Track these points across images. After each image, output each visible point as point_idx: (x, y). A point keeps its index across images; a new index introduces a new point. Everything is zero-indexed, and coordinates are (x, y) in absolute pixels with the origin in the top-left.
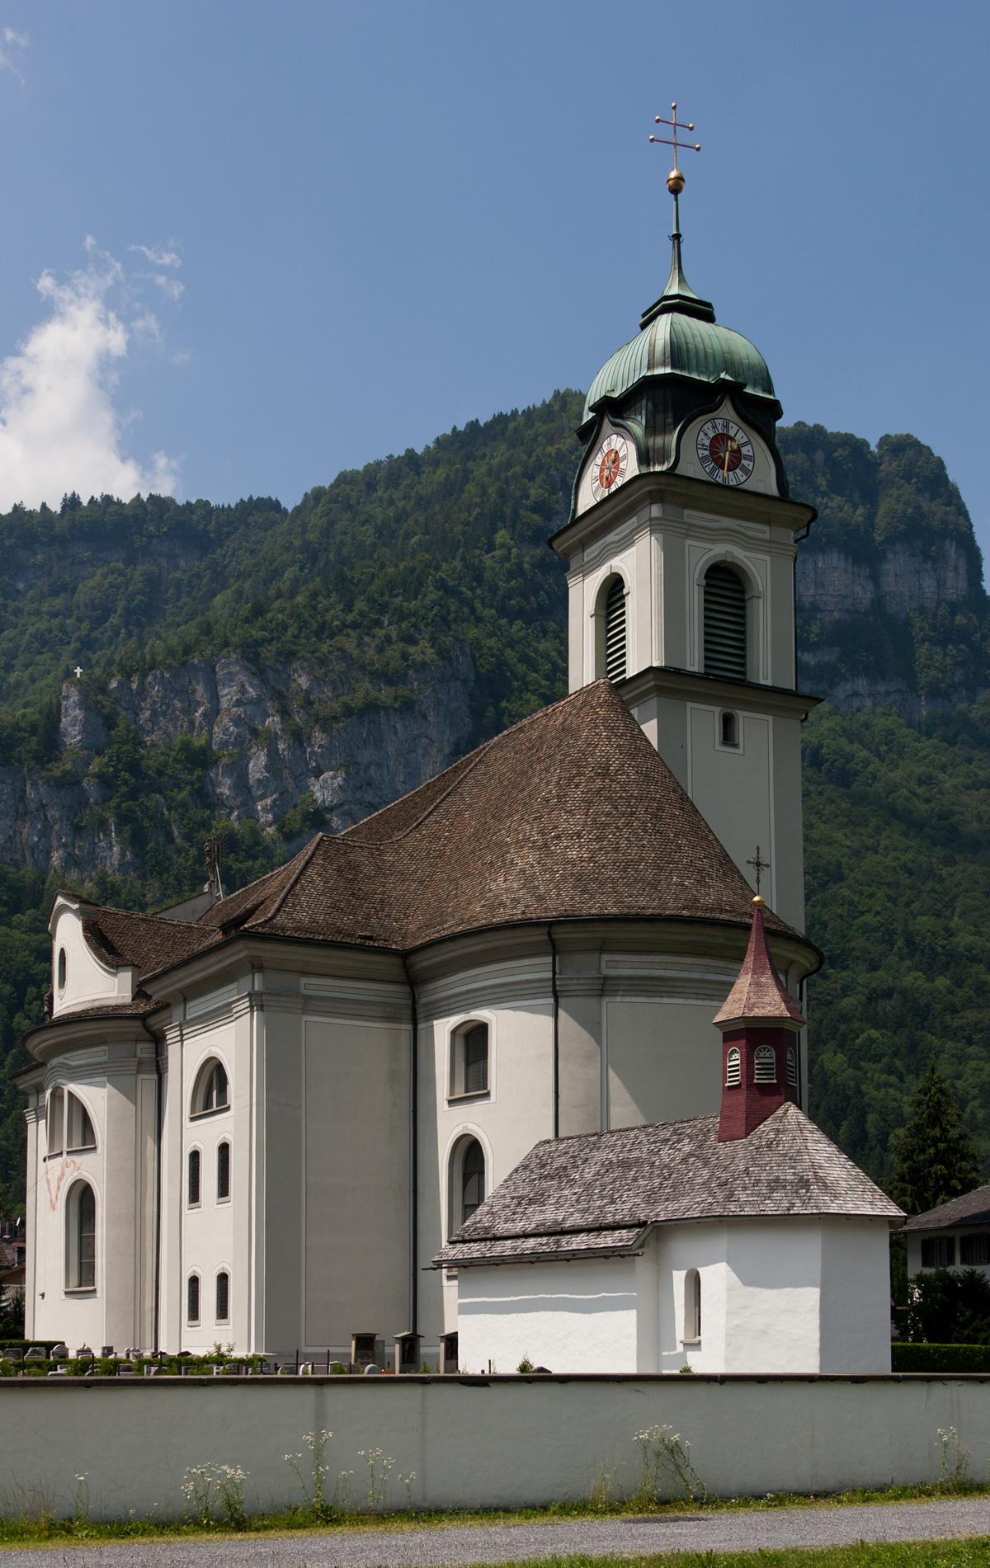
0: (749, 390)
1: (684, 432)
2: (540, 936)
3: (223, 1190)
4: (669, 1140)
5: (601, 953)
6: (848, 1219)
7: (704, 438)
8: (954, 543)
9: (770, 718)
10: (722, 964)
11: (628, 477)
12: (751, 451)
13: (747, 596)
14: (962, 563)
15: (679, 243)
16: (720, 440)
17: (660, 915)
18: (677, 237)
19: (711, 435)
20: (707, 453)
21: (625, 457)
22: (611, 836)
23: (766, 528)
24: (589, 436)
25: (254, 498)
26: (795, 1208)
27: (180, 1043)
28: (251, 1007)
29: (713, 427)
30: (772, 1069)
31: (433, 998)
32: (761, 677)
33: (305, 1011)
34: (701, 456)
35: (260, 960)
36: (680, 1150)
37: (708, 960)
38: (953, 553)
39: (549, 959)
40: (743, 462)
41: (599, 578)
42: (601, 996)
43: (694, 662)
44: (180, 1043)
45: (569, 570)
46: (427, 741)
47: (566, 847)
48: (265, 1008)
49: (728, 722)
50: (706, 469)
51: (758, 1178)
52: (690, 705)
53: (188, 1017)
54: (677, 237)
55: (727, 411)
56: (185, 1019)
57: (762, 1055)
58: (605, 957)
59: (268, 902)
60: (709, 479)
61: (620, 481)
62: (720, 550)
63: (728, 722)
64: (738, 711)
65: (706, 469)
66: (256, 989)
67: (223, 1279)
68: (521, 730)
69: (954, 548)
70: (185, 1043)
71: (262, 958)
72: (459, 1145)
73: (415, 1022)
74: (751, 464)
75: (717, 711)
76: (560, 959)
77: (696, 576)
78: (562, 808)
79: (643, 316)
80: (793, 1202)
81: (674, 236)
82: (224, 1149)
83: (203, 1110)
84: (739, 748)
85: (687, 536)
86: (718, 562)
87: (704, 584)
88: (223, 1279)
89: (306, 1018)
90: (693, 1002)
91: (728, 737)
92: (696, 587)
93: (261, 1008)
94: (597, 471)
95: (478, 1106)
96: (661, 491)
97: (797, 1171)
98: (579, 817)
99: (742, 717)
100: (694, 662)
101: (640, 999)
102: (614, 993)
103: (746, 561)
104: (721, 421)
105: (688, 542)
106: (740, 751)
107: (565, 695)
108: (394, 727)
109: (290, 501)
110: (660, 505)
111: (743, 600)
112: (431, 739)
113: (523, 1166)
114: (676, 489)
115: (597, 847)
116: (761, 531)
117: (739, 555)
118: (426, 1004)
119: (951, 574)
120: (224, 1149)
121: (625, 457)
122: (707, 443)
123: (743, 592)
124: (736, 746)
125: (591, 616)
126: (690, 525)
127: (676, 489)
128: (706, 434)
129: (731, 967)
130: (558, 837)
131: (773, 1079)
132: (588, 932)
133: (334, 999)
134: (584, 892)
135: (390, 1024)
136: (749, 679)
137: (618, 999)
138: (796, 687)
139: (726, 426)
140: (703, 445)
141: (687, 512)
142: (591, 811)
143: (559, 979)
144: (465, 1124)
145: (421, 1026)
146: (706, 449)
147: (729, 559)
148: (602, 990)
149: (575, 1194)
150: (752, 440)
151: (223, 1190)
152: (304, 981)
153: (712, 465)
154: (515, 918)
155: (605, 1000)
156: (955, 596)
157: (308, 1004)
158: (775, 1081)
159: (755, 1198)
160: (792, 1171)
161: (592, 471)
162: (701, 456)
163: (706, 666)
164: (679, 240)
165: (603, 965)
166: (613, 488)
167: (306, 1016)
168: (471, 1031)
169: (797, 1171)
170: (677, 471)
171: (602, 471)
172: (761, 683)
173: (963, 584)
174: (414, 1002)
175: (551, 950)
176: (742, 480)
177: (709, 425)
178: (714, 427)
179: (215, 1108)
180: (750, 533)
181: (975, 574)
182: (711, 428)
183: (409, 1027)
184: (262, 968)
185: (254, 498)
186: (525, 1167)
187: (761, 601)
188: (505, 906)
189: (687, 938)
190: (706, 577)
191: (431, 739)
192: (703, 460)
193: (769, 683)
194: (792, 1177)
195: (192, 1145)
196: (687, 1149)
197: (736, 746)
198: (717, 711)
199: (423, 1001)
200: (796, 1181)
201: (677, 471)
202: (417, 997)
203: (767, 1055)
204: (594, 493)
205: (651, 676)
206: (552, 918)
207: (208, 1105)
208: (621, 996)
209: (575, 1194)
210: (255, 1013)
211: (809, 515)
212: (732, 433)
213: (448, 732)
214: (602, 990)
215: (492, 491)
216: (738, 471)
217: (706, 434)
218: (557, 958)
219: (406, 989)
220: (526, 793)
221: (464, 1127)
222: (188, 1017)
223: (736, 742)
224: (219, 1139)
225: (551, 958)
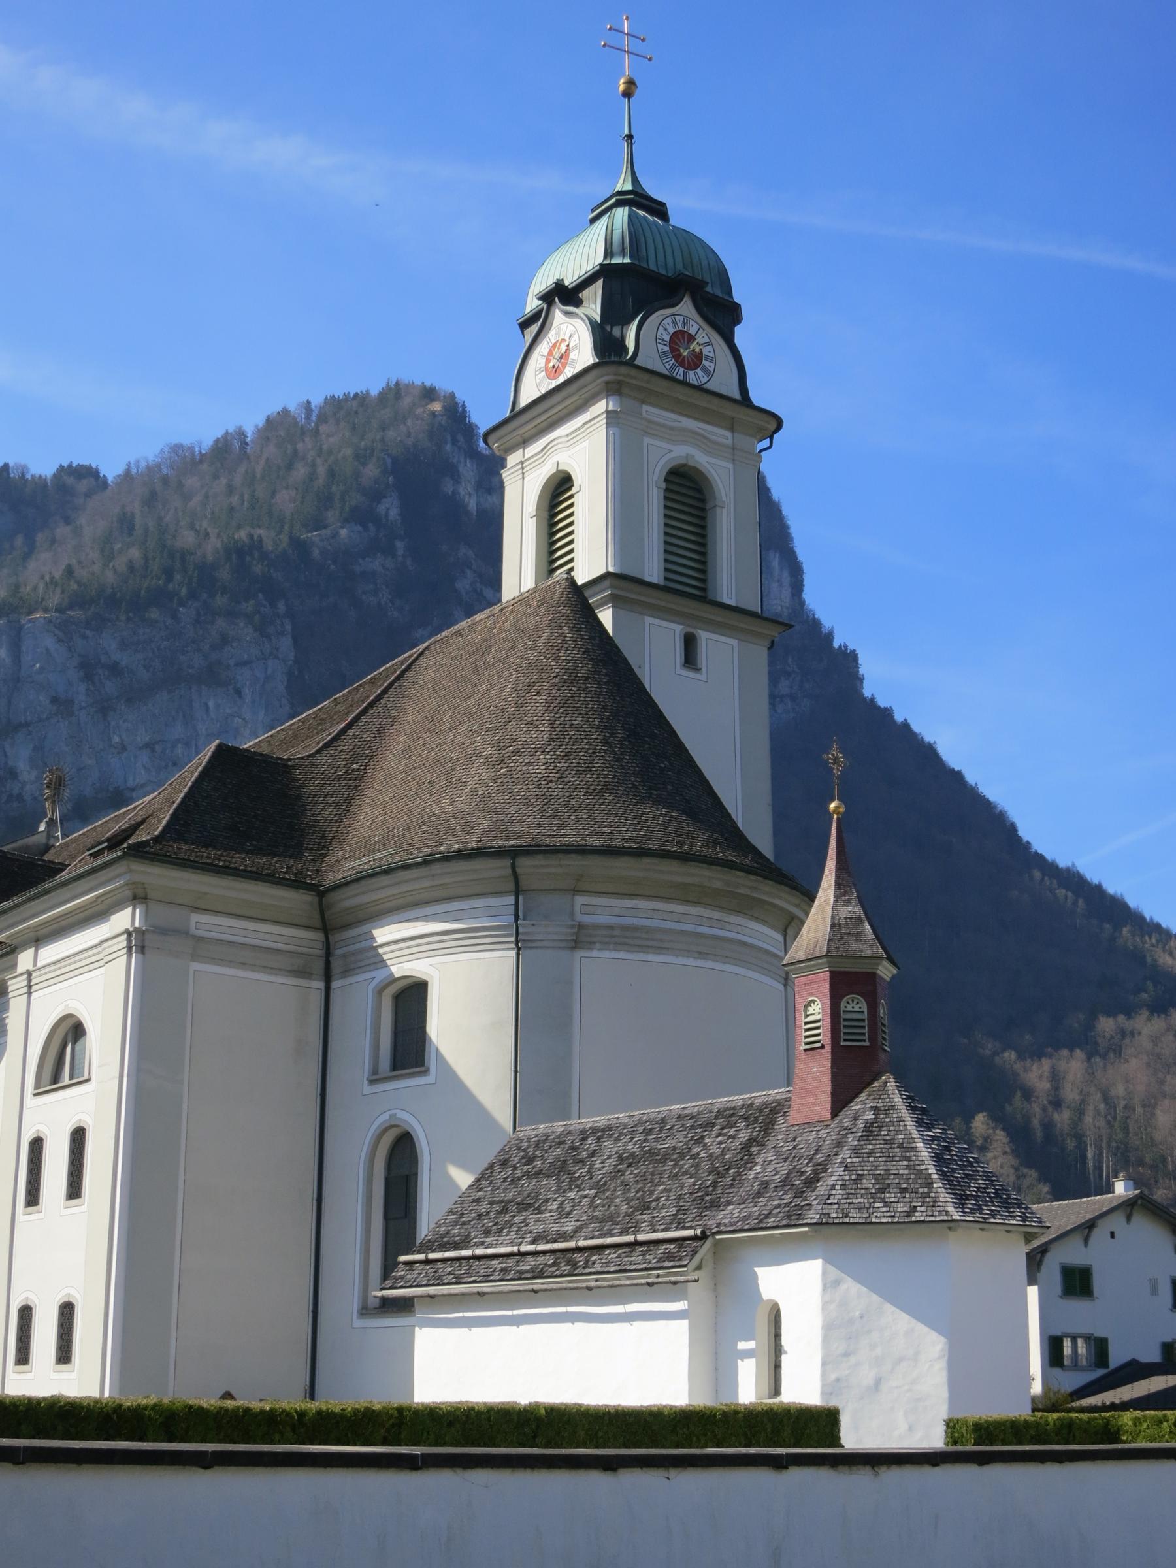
0: (709, 289)
1: (644, 323)
2: (501, 867)
3: (74, 1190)
4: (714, 1125)
5: (574, 895)
6: (1008, 1231)
7: (664, 332)
8: (777, 555)
9: (734, 642)
10: (717, 915)
11: (579, 367)
12: (712, 351)
13: (708, 506)
14: (786, 574)
15: (631, 144)
16: (681, 338)
17: (650, 849)
18: (630, 137)
19: (672, 331)
20: (667, 348)
21: (577, 347)
22: (582, 754)
23: (728, 434)
24: (536, 322)
25: (74, 465)
26: (917, 1214)
27: (26, 995)
28: (129, 948)
29: (673, 323)
30: (845, 1027)
31: (357, 946)
32: (725, 596)
33: (195, 957)
34: (660, 351)
35: (145, 888)
36: (733, 1137)
37: (702, 910)
38: (777, 566)
39: (511, 900)
40: (704, 362)
41: (542, 476)
42: (573, 948)
43: (654, 572)
44: (26, 995)
45: (506, 467)
46: (240, 720)
47: (529, 764)
48: (147, 950)
49: (690, 642)
50: (667, 365)
51: (860, 1173)
52: (648, 620)
53: (40, 964)
54: (630, 137)
55: (686, 307)
56: (35, 964)
57: (849, 1008)
58: (580, 900)
59: (153, 821)
60: (667, 373)
61: (569, 372)
62: (680, 452)
63: (690, 642)
64: (699, 631)
65: (667, 365)
66: (137, 925)
67: (67, 1311)
68: (458, 633)
69: (777, 559)
70: (34, 996)
71: (146, 886)
72: (382, 1141)
73: (328, 978)
74: (713, 365)
75: (677, 630)
76: (524, 899)
77: (656, 478)
78: (521, 719)
79: (593, 211)
80: (914, 1204)
81: (627, 136)
82: (78, 1137)
83: (51, 1085)
84: (701, 674)
85: (647, 433)
86: (676, 465)
87: (664, 487)
88: (67, 1311)
89: (195, 966)
90: (691, 962)
91: (690, 658)
92: (655, 490)
93: (142, 949)
94: (542, 362)
95: (408, 1084)
96: (620, 383)
97: (912, 1163)
98: (542, 729)
99: (706, 639)
100: (654, 572)
101: (622, 955)
102: (590, 945)
103: (708, 466)
104: (681, 318)
105: (647, 440)
106: (703, 677)
107: (500, 600)
108: (206, 704)
109: (111, 471)
110: (617, 397)
111: (703, 510)
112: (244, 719)
113: (500, 1161)
114: (634, 382)
115: (566, 765)
116: (721, 435)
117: (703, 460)
118: (344, 956)
119: (775, 585)
120: (78, 1137)
121: (577, 347)
122: (667, 338)
123: (703, 501)
124: (698, 670)
125: (532, 518)
126: (650, 421)
127: (634, 382)
128: (666, 329)
129: (727, 920)
130: (516, 752)
131: (864, 1041)
132: (561, 866)
133: (231, 943)
134: (554, 816)
135: (301, 980)
136: (710, 597)
137: (595, 953)
138: (762, 610)
139: (686, 323)
140: (663, 340)
141: (645, 408)
142: (558, 722)
143: (524, 926)
144: (391, 1112)
145: (335, 984)
146: (665, 345)
147: (691, 463)
148: (575, 941)
149: (586, 1197)
150: (713, 341)
151: (74, 1190)
152: (196, 918)
153: (672, 362)
154: (469, 846)
155: (580, 954)
156: (780, 608)
157: (201, 948)
158: (867, 1044)
159: (862, 1201)
160: (905, 1163)
161: (537, 360)
162: (660, 351)
163: (666, 579)
164: (631, 141)
165: (577, 909)
166: (561, 379)
167: (195, 963)
168: (403, 992)
169: (912, 1163)
170: (636, 362)
171: (548, 361)
172: (724, 602)
173: (786, 593)
174: (328, 954)
175: (513, 889)
176: (704, 381)
177: (669, 320)
178: (675, 323)
179: (66, 1080)
180: (712, 437)
181: (797, 586)
182: (671, 324)
183: (320, 985)
184: (146, 898)
185: (74, 465)
186: (504, 1163)
187: (724, 511)
188: (455, 834)
189: (679, 879)
190: (666, 480)
191: (244, 719)
192: (662, 355)
193: (732, 603)
194: (906, 1172)
195: (33, 1130)
196: (744, 1136)
197: (698, 670)
198: (677, 630)
199: (339, 952)
200: (913, 1176)
201: (636, 362)
202: (331, 947)
203: (857, 1008)
204: (538, 386)
205: (607, 583)
206: (509, 847)
207: (56, 1078)
208: (599, 949)
209: (586, 1197)
210: (134, 955)
211: (773, 426)
212: (692, 331)
213: (263, 712)
214: (575, 941)
215: (322, 470)
216: (698, 370)
217: (666, 329)
218: (521, 898)
219: (320, 936)
220: (472, 701)
221: (391, 1116)
222: (40, 964)
223: (699, 666)
224: (73, 1121)
225: (513, 897)
